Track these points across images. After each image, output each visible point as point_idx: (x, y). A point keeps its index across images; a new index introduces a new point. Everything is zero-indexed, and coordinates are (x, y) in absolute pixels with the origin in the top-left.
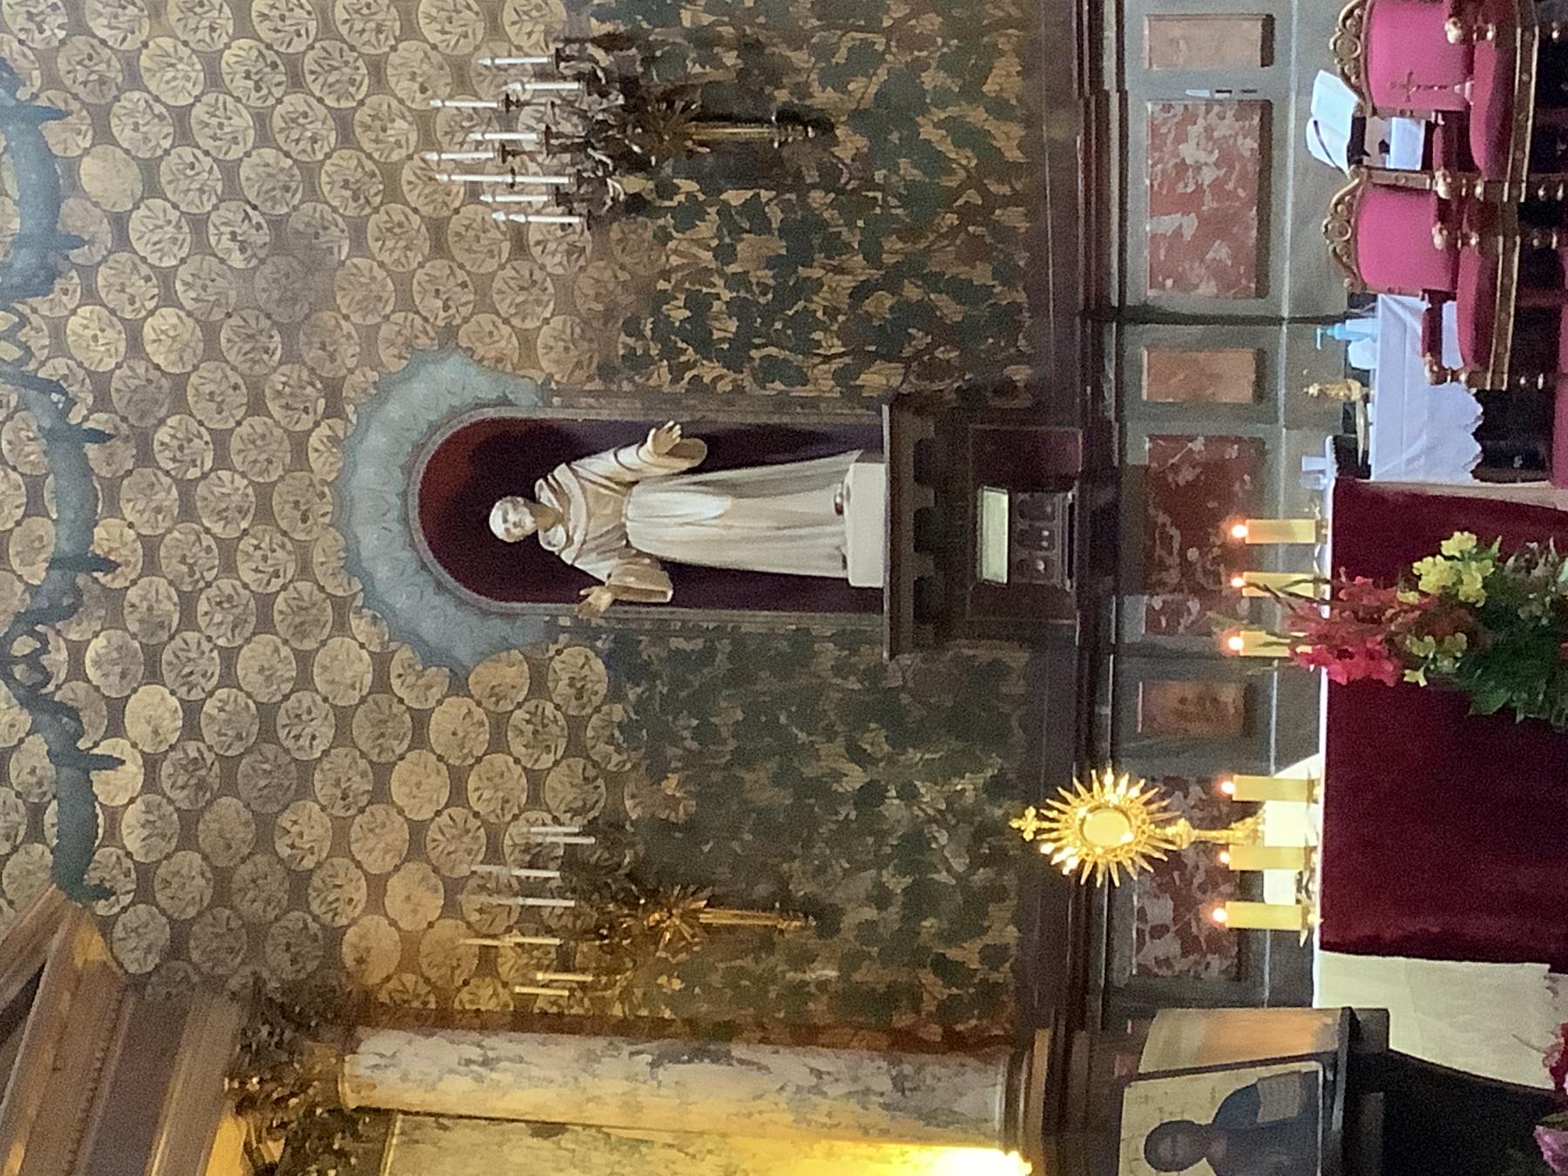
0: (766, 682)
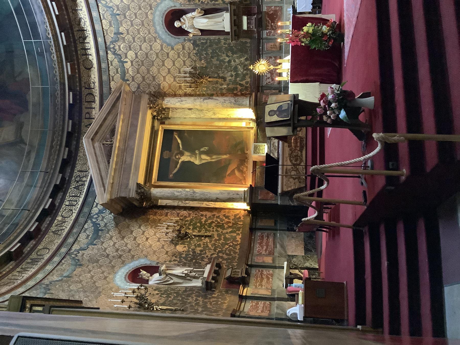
0: (215, 46)
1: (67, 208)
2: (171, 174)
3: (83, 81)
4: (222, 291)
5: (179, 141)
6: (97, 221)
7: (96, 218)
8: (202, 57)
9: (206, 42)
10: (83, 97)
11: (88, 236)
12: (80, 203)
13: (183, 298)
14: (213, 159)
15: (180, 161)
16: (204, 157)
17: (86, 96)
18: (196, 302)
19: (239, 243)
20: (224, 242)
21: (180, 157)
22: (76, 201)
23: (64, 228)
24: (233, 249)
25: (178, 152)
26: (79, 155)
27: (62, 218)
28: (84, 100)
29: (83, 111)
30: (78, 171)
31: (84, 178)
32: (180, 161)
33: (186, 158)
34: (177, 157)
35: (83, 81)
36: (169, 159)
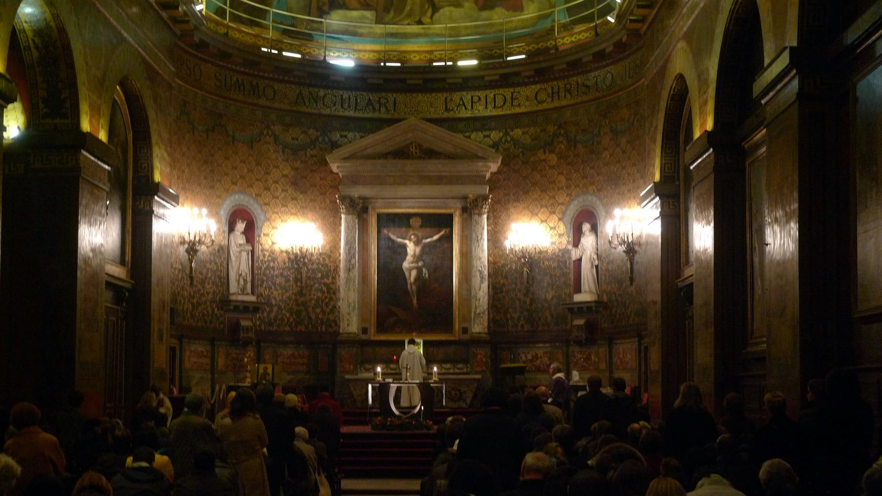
1: (337, 98)
2: (388, 231)
3: (521, 90)
4: (222, 317)
5: (436, 237)
6: (319, 142)
7: (324, 140)
8: (552, 262)
9: (566, 268)
10: (501, 91)
11: (297, 139)
12: (347, 113)
13: (210, 278)
14: (411, 286)
15: (407, 242)
16: (414, 273)
17: (502, 94)
18: (205, 293)
19: (294, 329)
20: (295, 310)
21: (413, 240)
22: (349, 106)
23: (307, 104)
24: (285, 323)
25: (420, 237)
26: (419, 94)
27: (322, 96)
28: (497, 91)
29: (481, 92)
30: (395, 99)
31: (384, 109)
32: (407, 242)
33: (412, 248)
34: (413, 237)
35: (521, 90)
36: (409, 226)
